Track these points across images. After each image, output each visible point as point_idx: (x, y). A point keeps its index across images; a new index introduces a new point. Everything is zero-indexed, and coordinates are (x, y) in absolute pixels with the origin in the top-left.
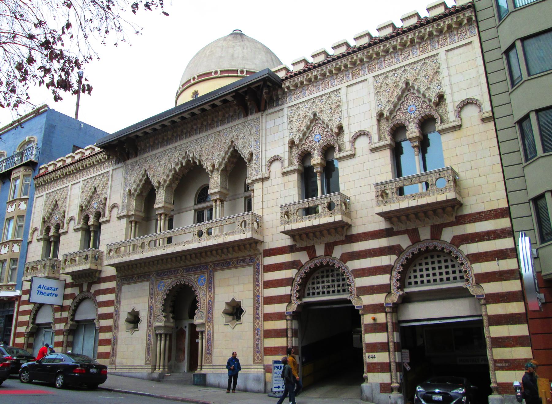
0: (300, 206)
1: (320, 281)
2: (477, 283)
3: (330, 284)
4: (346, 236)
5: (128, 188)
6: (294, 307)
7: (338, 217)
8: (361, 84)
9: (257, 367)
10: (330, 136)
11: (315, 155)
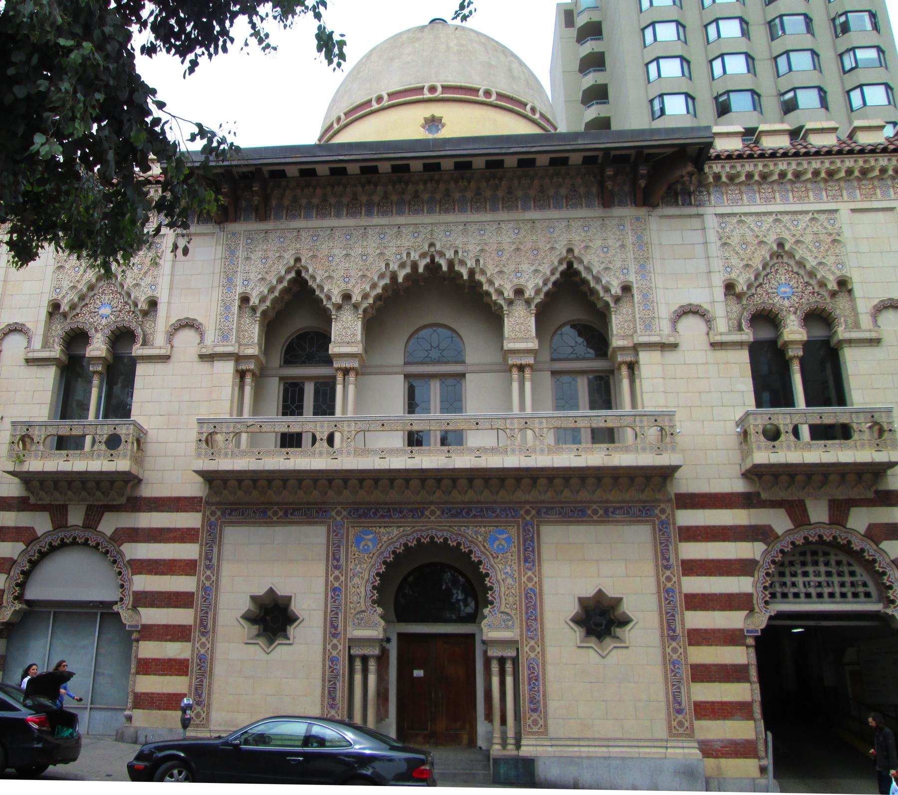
0: (52, 431)
1: (799, 572)
2: (134, 607)
3: (822, 579)
4: (877, 492)
5: (239, 290)
6: (760, 621)
7: (122, 465)
8: (880, 215)
9: (680, 744)
10: (129, 312)
11: (95, 340)
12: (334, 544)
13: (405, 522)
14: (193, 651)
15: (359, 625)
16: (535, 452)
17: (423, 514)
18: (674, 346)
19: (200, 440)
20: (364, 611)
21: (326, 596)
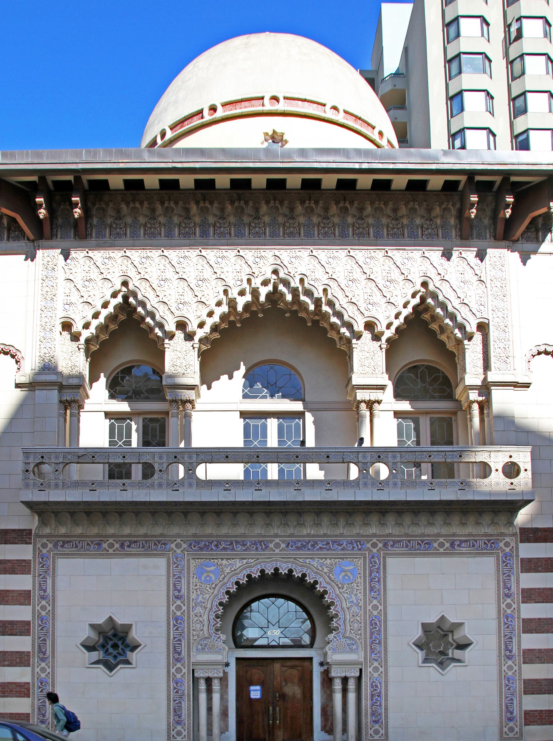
12: (174, 575)
13: (248, 555)
14: (33, 675)
15: (203, 650)
16: (183, 486)
17: (267, 547)
18: (527, 386)
19: (27, 471)
20: (206, 638)
21: (169, 624)
